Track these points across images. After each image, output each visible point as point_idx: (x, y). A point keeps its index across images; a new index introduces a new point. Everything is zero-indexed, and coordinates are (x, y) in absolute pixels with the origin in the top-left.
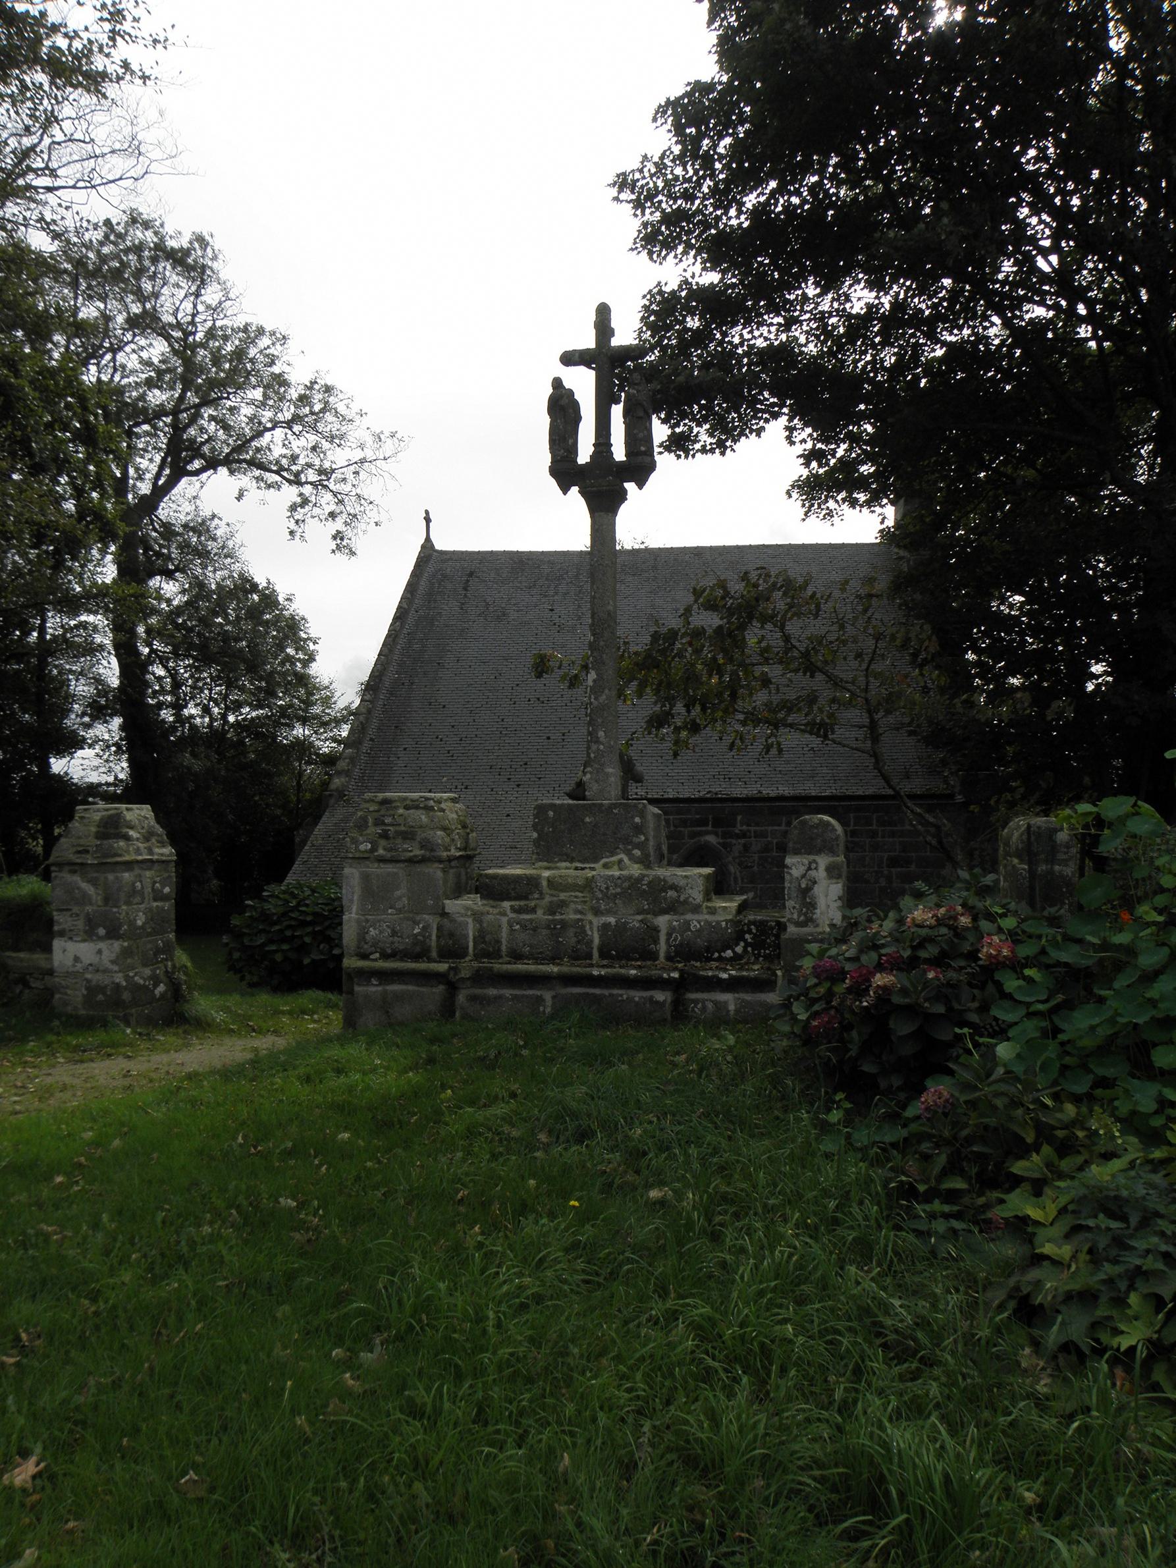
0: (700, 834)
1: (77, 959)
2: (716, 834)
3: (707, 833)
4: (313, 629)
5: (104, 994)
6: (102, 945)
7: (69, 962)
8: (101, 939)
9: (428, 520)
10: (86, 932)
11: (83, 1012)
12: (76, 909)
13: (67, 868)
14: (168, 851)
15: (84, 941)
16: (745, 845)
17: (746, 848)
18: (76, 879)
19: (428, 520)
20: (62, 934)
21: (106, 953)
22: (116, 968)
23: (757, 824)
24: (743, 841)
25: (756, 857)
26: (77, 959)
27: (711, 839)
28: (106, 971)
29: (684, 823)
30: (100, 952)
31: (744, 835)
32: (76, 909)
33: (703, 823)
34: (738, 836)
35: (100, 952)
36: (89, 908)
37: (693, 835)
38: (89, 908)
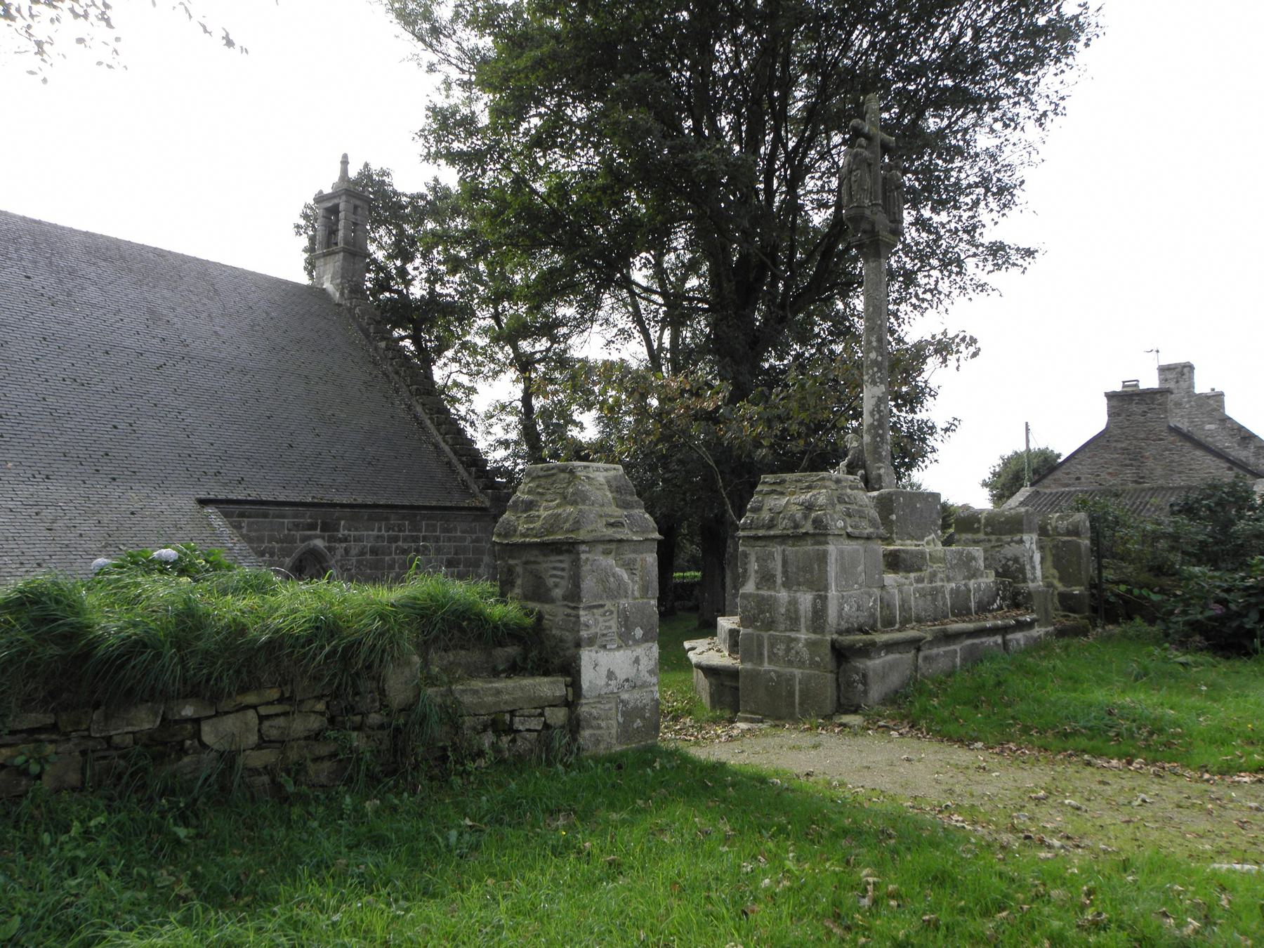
0: (309, 538)
1: (611, 675)
2: (323, 538)
3: (316, 537)
4: (1008, 453)
5: (643, 718)
6: (640, 651)
7: (602, 681)
8: (637, 642)
9: (1027, 430)
10: (620, 636)
11: (618, 748)
12: (609, 605)
13: (601, 547)
14: (656, 535)
15: (619, 647)
16: (346, 549)
17: (347, 551)
18: (610, 561)
19: (1027, 430)
20: (591, 642)
21: (644, 661)
22: (654, 680)
23: (356, 530)
24: (344, 545)
25: (354, 560)
26: (611, 675)
27: (319, 543)
28: (644, 685)
29: (296, 526)
30: (637, 661)
31: (345, 540)
32: (609, 605)
33: (312, 527)
34: (341, 541)
35: (637, 661)
36: (624, 603)
37: (303, 541)
38: (624, 603)
